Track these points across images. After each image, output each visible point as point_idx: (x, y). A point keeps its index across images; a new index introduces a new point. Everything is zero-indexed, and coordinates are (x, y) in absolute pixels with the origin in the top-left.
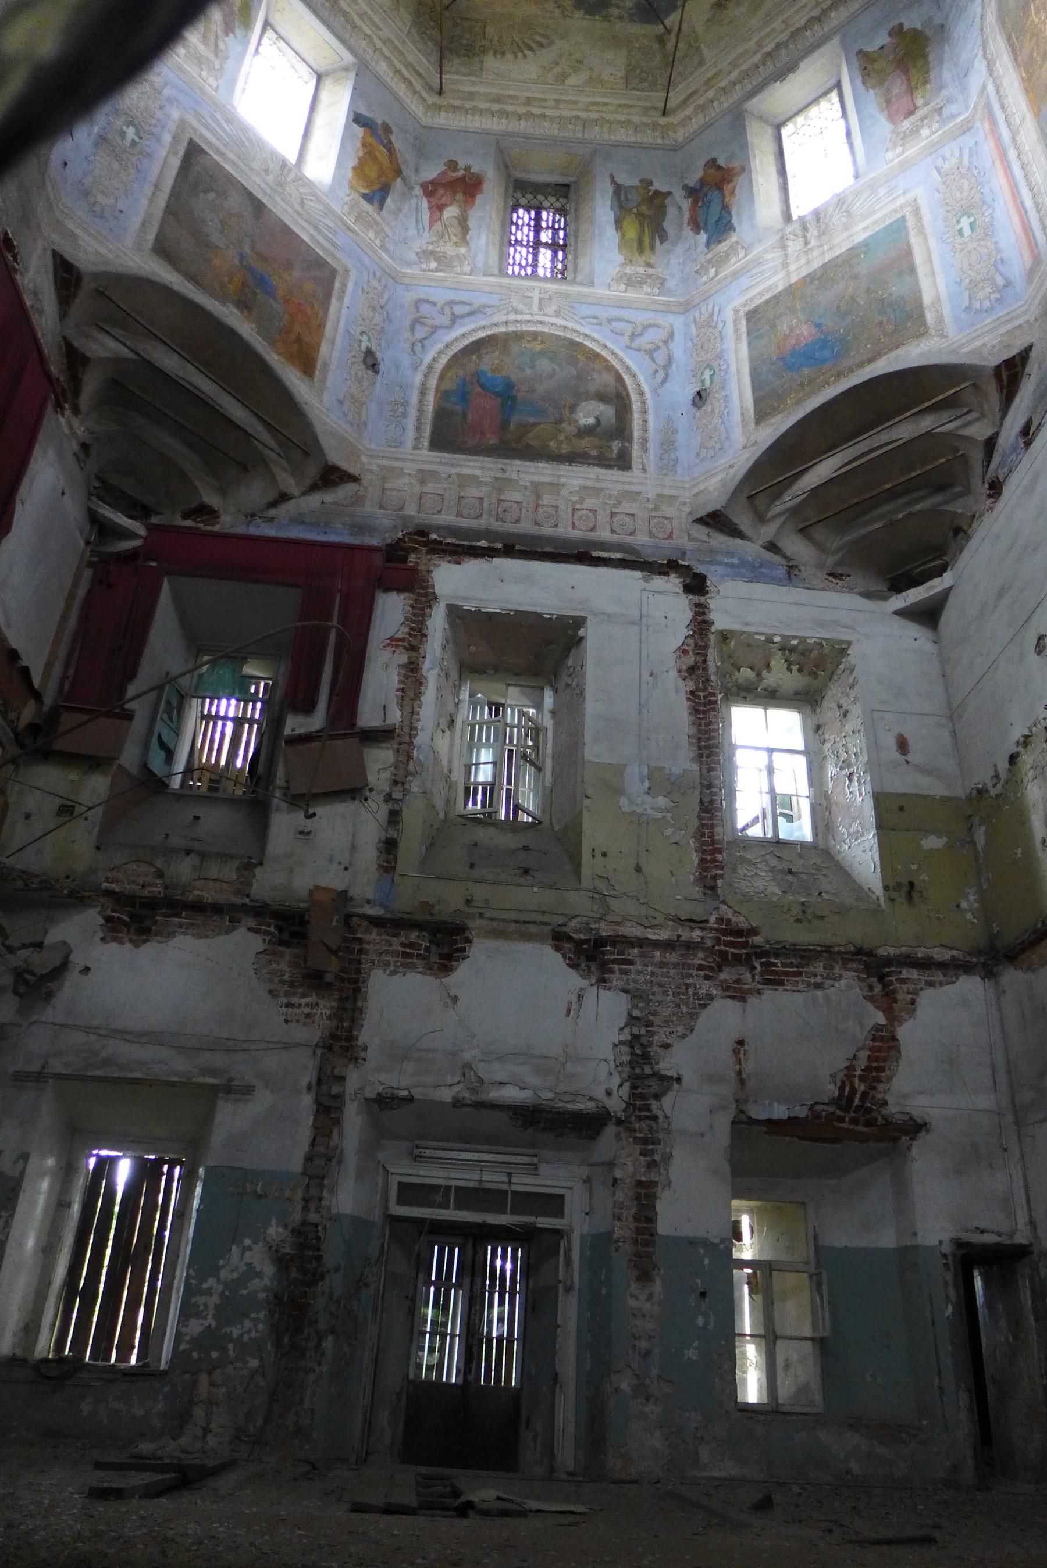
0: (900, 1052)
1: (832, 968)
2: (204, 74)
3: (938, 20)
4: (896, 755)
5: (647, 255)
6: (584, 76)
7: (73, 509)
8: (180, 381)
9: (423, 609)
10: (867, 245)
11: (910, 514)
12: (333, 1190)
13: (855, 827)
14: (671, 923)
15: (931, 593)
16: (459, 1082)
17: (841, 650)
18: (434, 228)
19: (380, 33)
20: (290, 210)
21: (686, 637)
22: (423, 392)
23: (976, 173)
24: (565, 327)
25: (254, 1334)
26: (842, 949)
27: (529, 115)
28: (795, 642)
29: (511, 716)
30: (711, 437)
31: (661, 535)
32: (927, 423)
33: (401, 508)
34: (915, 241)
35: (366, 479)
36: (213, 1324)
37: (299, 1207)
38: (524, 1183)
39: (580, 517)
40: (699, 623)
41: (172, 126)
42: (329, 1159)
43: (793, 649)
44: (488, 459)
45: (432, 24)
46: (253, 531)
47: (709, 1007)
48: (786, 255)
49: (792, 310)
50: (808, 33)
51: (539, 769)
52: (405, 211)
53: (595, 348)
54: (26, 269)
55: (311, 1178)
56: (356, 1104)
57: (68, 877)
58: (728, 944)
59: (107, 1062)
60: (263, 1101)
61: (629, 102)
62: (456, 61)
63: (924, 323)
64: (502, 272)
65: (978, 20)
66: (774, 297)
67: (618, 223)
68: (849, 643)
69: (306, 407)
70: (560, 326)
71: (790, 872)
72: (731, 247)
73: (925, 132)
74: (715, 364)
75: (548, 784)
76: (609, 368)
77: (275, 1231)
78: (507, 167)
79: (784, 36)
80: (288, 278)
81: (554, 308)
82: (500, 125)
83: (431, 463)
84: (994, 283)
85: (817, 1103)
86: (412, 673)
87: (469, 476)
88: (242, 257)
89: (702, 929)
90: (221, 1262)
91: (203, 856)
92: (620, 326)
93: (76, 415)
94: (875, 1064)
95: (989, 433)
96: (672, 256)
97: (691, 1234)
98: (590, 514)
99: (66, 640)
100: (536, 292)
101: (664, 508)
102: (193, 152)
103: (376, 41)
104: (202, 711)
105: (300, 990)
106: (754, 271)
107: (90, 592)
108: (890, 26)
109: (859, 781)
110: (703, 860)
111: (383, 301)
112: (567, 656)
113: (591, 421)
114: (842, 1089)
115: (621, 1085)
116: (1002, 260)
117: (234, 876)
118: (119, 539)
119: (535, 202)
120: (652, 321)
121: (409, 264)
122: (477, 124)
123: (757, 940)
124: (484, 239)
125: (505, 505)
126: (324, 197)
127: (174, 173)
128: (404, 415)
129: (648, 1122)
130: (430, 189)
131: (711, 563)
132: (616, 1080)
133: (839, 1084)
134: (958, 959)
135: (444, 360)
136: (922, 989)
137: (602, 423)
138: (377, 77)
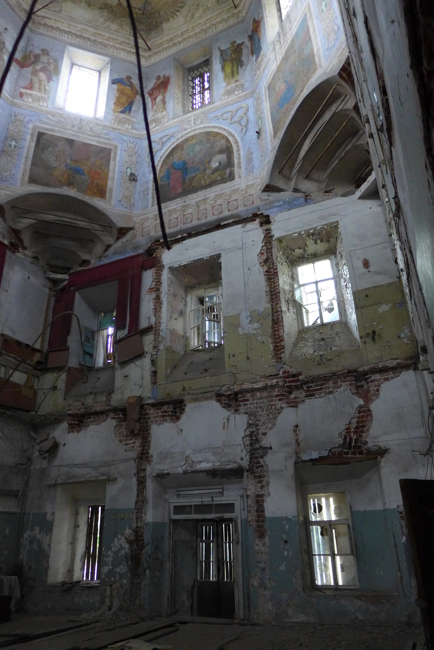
0: (372, 416)
1: (337, 382)
2: (41, 104)
8: (56, 222)
9: (160, 273)
12: (145, 514)
14: (263, 379)
16: (185, 464)
17: (335, 226)
20: (86, 136)
21: (262, 247)
24: (204, 127)
25: (124, 571)
26: (341, 372)
27: (184, 39)
28: (312, 231)
35: (137, 226)
36: (111, 568)
37: (135, 521)
38: (218, 500)
41: (30, 131)
42: (143, 502)
43: (313, 234)
44: (179, 199)
46: (102, 263)
47: (282, 413)
55: (138, 509)
56: (150, 479)
58: (289, 382)
59: (74, 476)
60: (121, 482)
68: (337, 222)
70: (203, 128)
76: (223, 137)
77: (128, 532)
80: (89, 163)
81: (200, 120)
85: (333, 448)
86: (158, 300)
88: (66, 165)
89: (276, 378)
90: (112, 545)
91: (95, 394)
93: (26, 250)
94: (361, 424)
95: (353, 104)
97: (280, 515)
103: (116, 45)
105: (129, 438)
111: (135, 151)
113: (217, 164)
114: (345, 439)
115: (246, 455)
118: (62, 283)
120: (239, 107)
122: (166, 55)
123: (301, 378)
125: (186, 217)
128: (147, 194)
129: (261, 468)
131: (271, 208)
132: (245, 452)
133: (343, 437)
134: (401, 364)
136: (382, 383)
137: (222, 163)
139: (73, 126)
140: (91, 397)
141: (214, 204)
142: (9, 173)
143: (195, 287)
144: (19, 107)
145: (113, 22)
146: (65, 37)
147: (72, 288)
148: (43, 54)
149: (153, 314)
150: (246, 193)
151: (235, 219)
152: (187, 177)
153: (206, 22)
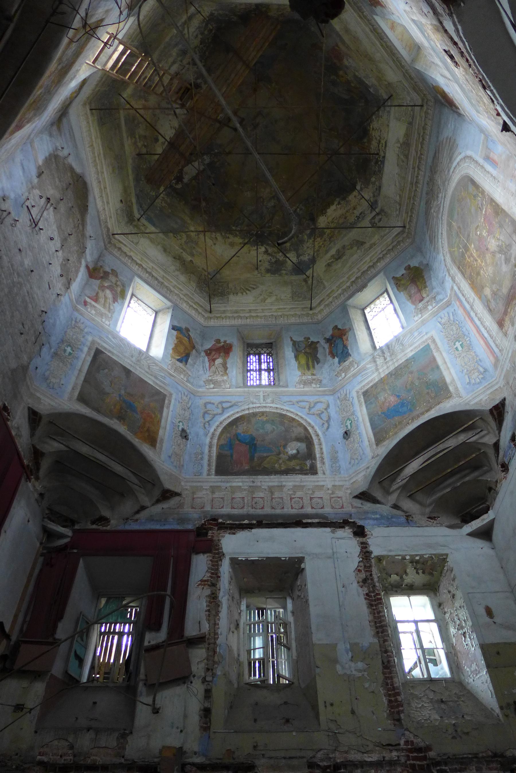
2: (104, 320)
3: (425, 262)
4: (487, 619)
6: (274, 298)
7: (34, 528)
9: (217, 562)
10: (414, 358)
11: (464, 483)
13: (474, 666)
14: (377, 748)
15: (485, 522)
17: (443, 559)
18: (211, 369)
20: (143, 372)
22: (210, 447)
23: (458, 322)
24: (277, 408)
26: (484, 755)
27: (251, 317)
28: (417, 558)
29: (270, 616)
30: (355, 454)
31: (337, 507)
32: (462, 438)
33: (203, 508)
34: (436, 354)
35: (184, 493)
39: (295, 502)
40: (365, 553)
41: (88, 344)
43: (417, 562)
45: (205, 285)
46: (128, 527)
48: (377, 365)
49: (384, 390)
50: (369, 272)
51: (289, 649)
52: (197, 363)
53: (292, 416)
54: (14, 418)
57: (17, 754)
58: (415, 758)
61: (296, 306)
62: (217, 299)
63: (449, 391)
64: (245, 385)
65: (443, 262)
66: (375, 384)
67: (296, 357)
68: (447, 555)
69: (152, 462)
71: (442, 701)
72: (350, 363)
73: (430, 307)
74: (351, 418)
75: (294, 658)
76: (300, 425)
78: (243, 338)
79: (359, 274)
80: (143, 402)
82: (239, 322)
83: (217, 482)
84: (479, 371)
86: (213, 599)
87: (237, 486)
88: (120, 396)
91: (97, 731)
92: (303, 404)
95: (494, 440)
96: (323, 369)
98: (300, 500)
99: (27, 598)
100: (261, 393)
102: (98, 353)
103: (181, 295)
104: (101, 630)
106: (363, 373)
107: (41, 571)
108: (404, 266)
109: (470, 638)
110: (390, 701)
111: (189, 406)
112: (296, 579)
113: (295, 452)
116: (480, 360)
117: (115, 744)
119: (257, 352)
120: (318, 400)
121: (200, 387)
122: (228, 323)
124: (235, 372)
125: (255, 500)
126: (159, 364)
127: (88, 364)
128: (202, 459)
130: (208, 353)
135: (220, 430)
137: (300, 452)
138: (182, 310)
139: (132, 356)
140: (91, 735)
141: (292, 494)
142: (58, 381)
143: (254, 592)
144: (81, 314)
145: (182, 274)
146: (136, 268)
147: (75, 551)
148: (112, 274)
149: (205, 618)
150: (333, 493)
151: (322, 521)
152: (256, 455)
153: (278, 310)
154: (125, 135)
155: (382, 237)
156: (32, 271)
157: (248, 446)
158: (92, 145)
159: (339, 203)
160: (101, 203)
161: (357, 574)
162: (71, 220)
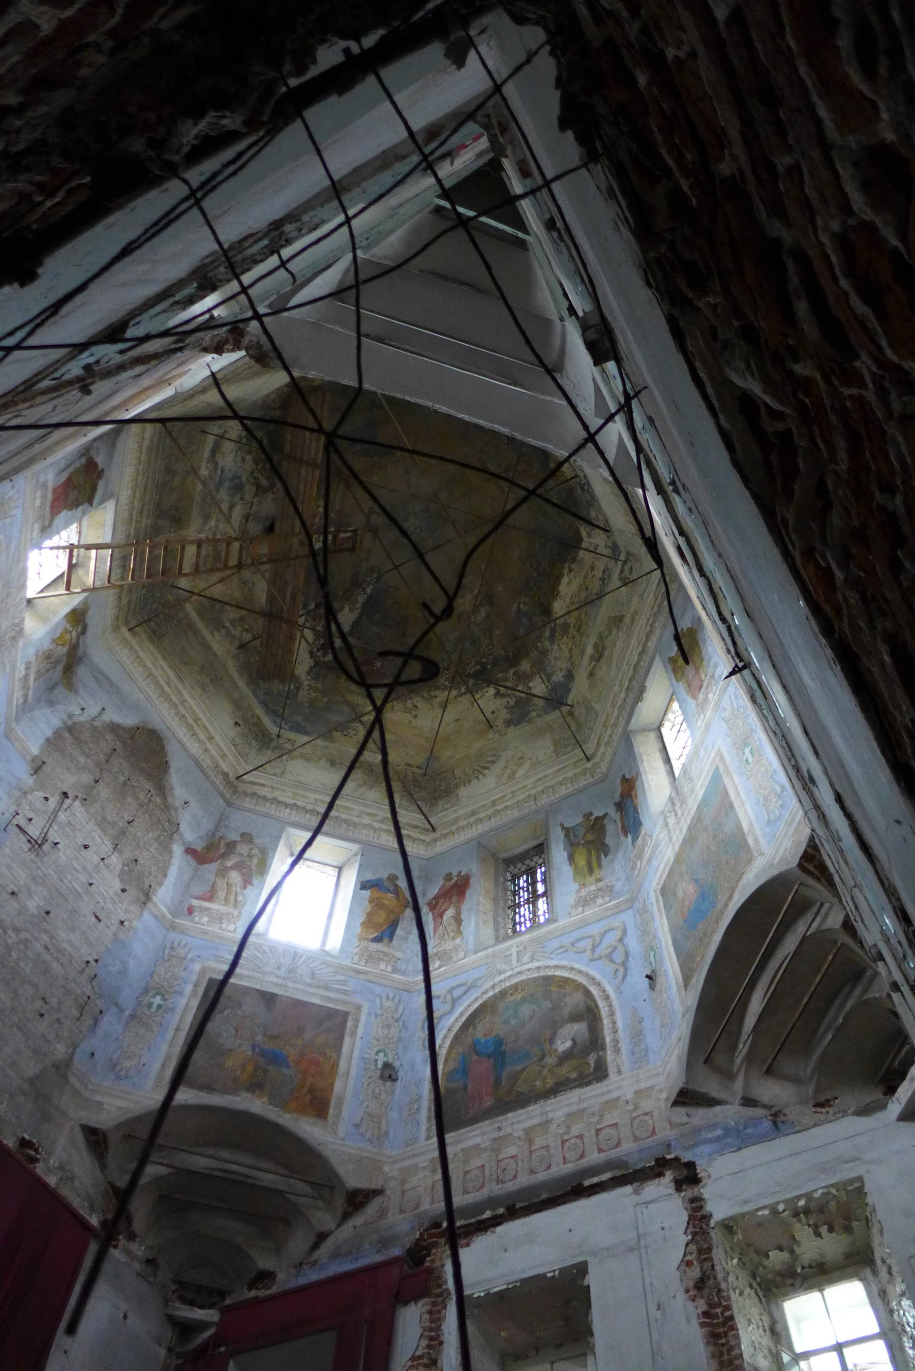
5: (597, 873)
19: (377, 818)
21: (687, 1245)
24: (539, 968)
28: (802, 1203)
31: (644, 1135)
33: (418, 1206)
43: (807, 1211)
46: (302, 1281)
50: (642, 664)
67: (571, 858)
68: (860, 1179)
69: (320, 1148)
73: (710, 696)
76: (578, 986)
79: (309, 807)
93: (134, 1240)
95: (841, 919)
98: (578, 1141)
101: (642, 1104)
113: (568, 1044)
120: (607, 928)
122: (463, 838)
125: (502, 1165)
128: (418, 1110)
131: (696, 1145)
137: (578, 1041)
139: (279, 968)
144: (183, 932)
147: (223, 1349)
148: (243, 841)
151: (617, 1173)
152: (505, 1074)
154: (206, 633)
155: (642, 596)
156: (48, 913)
157: (492, 1060)
158: (150, 674)
159: (570, 570)
160: (196, 745)
161: (685, 1272)
162: (129, 800)
